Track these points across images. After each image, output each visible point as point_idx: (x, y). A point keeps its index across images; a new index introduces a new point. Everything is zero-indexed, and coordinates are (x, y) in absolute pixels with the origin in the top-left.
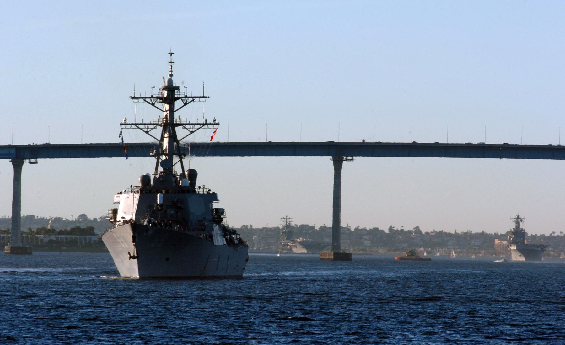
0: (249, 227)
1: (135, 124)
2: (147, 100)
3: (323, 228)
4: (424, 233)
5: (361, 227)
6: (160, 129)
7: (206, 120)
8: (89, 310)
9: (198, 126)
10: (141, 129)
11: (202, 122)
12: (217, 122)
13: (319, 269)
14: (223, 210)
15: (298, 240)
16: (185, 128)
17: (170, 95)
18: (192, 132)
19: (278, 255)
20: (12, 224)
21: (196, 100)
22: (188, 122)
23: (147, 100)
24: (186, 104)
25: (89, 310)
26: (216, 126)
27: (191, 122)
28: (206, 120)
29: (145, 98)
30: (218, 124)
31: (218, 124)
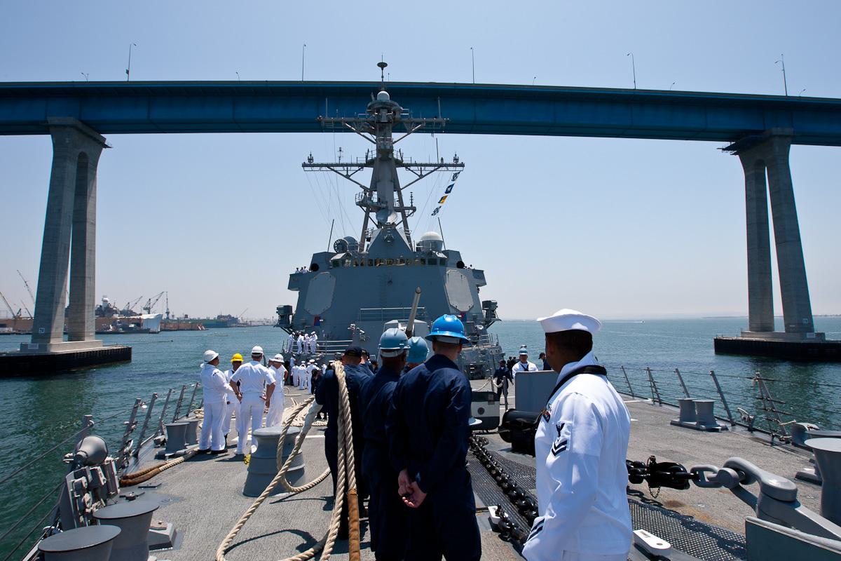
0: (165, 316)
1: (328, 166)
4: (109, 138)
5: (224, 314)
7: (442, 159)
9: (432, 168)
10: (336, 171)
11: (435, 162)
12: (460, 162)
13: (345, 435)
16: (409, 170)
18: (421, 177)
22: (413, 162)
26: (459, 169)
27: (418, 162)
28: (442, 159)
30: (462, 165)
31: (462, 165)
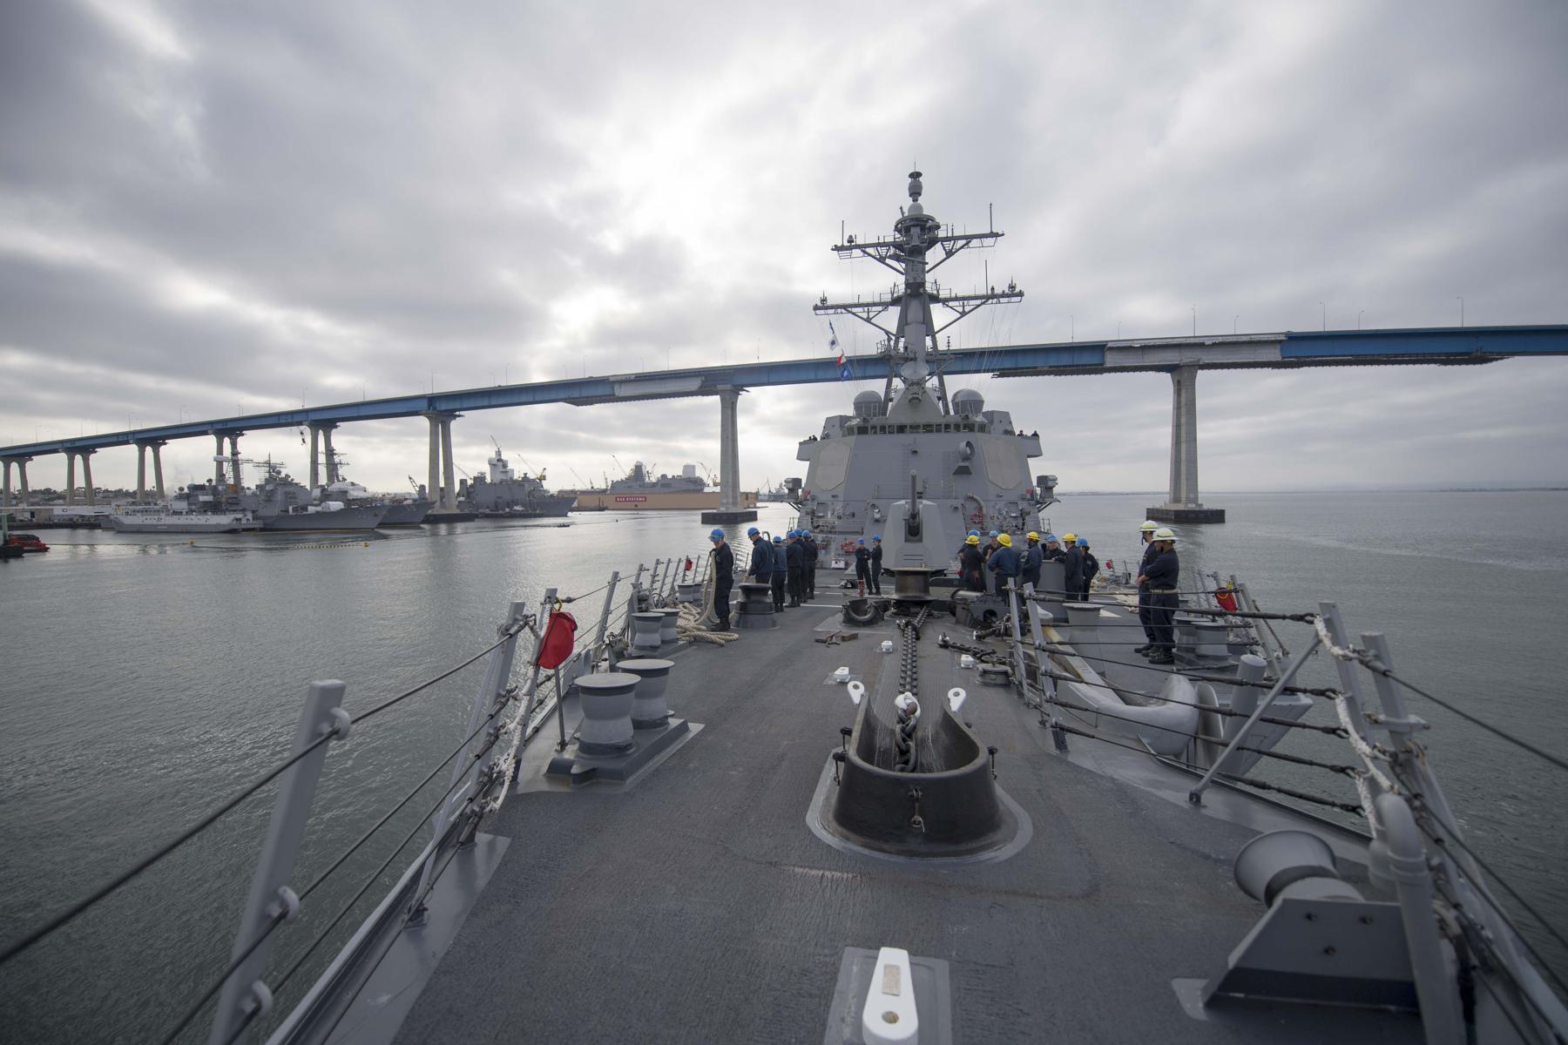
1: (845, 307)
2: (870, 250)
3: (777, 540)
6: (895, 311)
8: (68, 801)
14: (920, 540)
15: (856, 693)
17: (915, 238)
18: (963, 314)
19: (855, 969)
20: (1143, 588)
21: (975, 242)
23: (870, 250)
24: (949, 254)
25: (68, 801)
29: (862, 247)
